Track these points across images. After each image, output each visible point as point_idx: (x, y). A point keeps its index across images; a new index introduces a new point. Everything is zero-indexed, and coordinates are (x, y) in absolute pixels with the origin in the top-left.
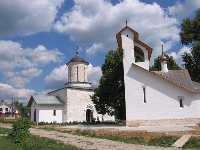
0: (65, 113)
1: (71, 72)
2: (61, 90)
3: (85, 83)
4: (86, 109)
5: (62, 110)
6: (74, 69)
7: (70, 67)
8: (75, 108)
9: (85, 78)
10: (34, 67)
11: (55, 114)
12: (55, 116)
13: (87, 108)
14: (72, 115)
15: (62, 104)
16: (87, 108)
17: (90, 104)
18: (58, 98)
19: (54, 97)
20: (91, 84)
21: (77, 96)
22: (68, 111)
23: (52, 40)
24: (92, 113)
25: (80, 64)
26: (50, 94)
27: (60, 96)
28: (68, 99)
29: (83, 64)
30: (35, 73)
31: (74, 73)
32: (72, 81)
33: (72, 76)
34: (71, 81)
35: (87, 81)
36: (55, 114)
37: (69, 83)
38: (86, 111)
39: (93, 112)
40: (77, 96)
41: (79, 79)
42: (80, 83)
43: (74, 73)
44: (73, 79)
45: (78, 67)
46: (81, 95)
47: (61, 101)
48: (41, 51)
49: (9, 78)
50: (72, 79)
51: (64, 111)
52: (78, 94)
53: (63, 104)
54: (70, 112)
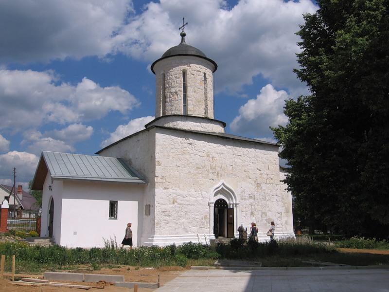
0: (147, 210)
1: (164, 89)
2: (134, 138)
3: (206, 119)
4: (214, 200)
5: (136, 203)
6: (176, 77)
7: (162, 72)
8: (181, 195)
9: (206, 106)
10: (78, 123)
11: (113, 213)
12: (113, 221)
13: (216, 194)
14: (171, 218)
15: (136, 180)
16: (216, 194)
17: (226, 184)
18: (125, 163)
19: (114, 159)
20: (224, 125)
21: (188, 157)
22: (156, 204)
23: (115, 70)
24: (231, 211)
25: (191, 65)
26: (104, 152)
27: (131, 156)
28: (156, 163)
29: (201, 66)
30: (80, 132)
31: (173, 90)
32: (168, 113)
33: (168, 100)
34: (166, 114)
35: (211, 116)
36: (113, 213)
37: (160, 118)
38: (213, 205)
39: (235, 208)
40: (188, 157)
41: (190, 107)
42: (194, 119)
43: (173, 90)
44: (170, 107)
45: (188, 72)
46: (200, 154)
47: (133, 173)
48: (91, 91)
49: (32, 142)
50: (168, 107)
51: (145, 205)
52: (189, 149)
53: (140, 181)
54: (163, 206)
